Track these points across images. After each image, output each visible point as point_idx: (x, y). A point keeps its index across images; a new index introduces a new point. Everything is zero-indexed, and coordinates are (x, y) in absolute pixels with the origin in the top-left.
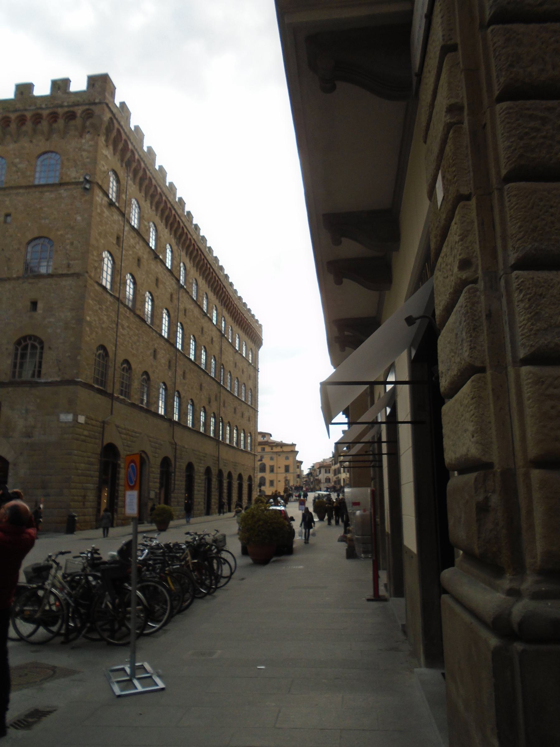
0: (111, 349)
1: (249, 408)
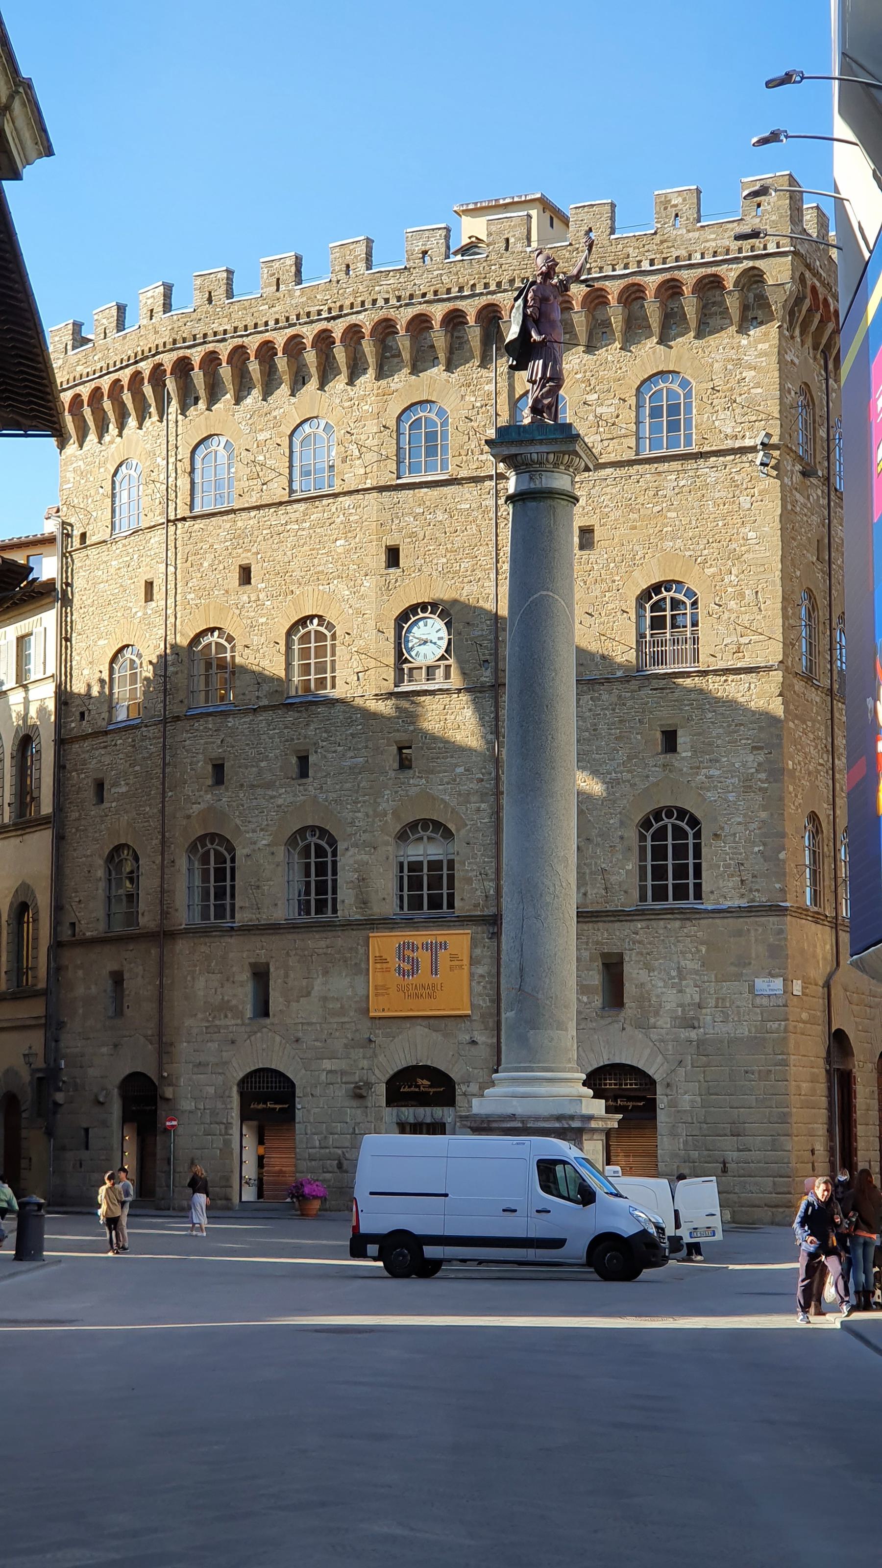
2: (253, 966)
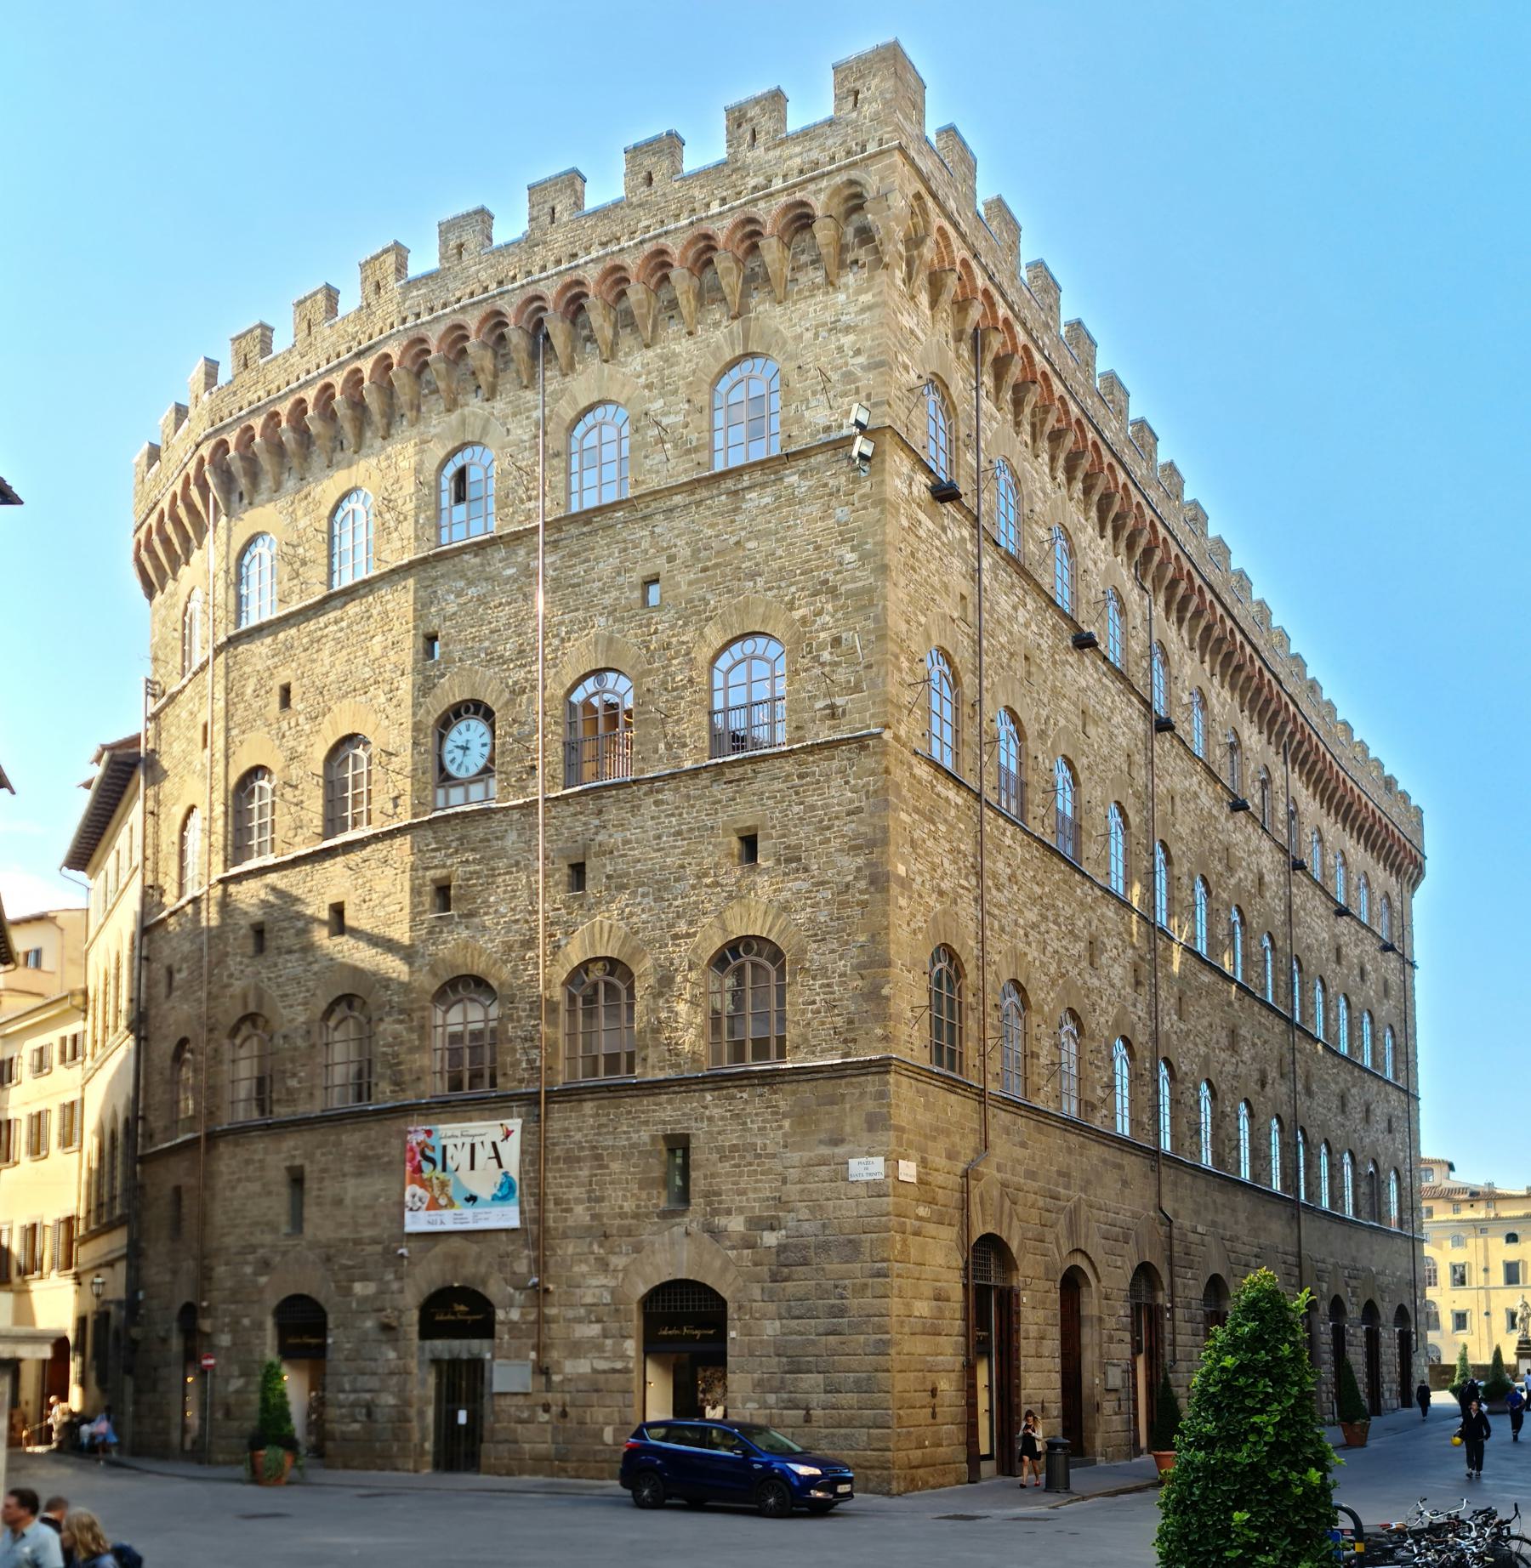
0: (968, 949)
1: (1389, 1089)
2: (290, 1169)
